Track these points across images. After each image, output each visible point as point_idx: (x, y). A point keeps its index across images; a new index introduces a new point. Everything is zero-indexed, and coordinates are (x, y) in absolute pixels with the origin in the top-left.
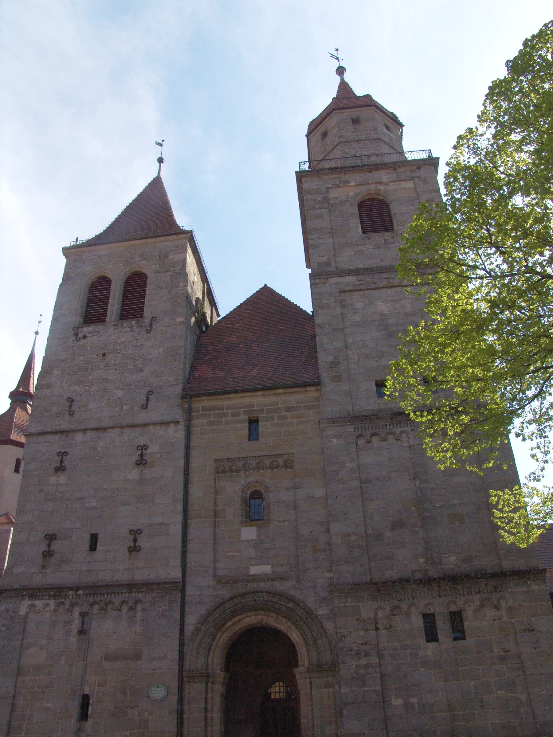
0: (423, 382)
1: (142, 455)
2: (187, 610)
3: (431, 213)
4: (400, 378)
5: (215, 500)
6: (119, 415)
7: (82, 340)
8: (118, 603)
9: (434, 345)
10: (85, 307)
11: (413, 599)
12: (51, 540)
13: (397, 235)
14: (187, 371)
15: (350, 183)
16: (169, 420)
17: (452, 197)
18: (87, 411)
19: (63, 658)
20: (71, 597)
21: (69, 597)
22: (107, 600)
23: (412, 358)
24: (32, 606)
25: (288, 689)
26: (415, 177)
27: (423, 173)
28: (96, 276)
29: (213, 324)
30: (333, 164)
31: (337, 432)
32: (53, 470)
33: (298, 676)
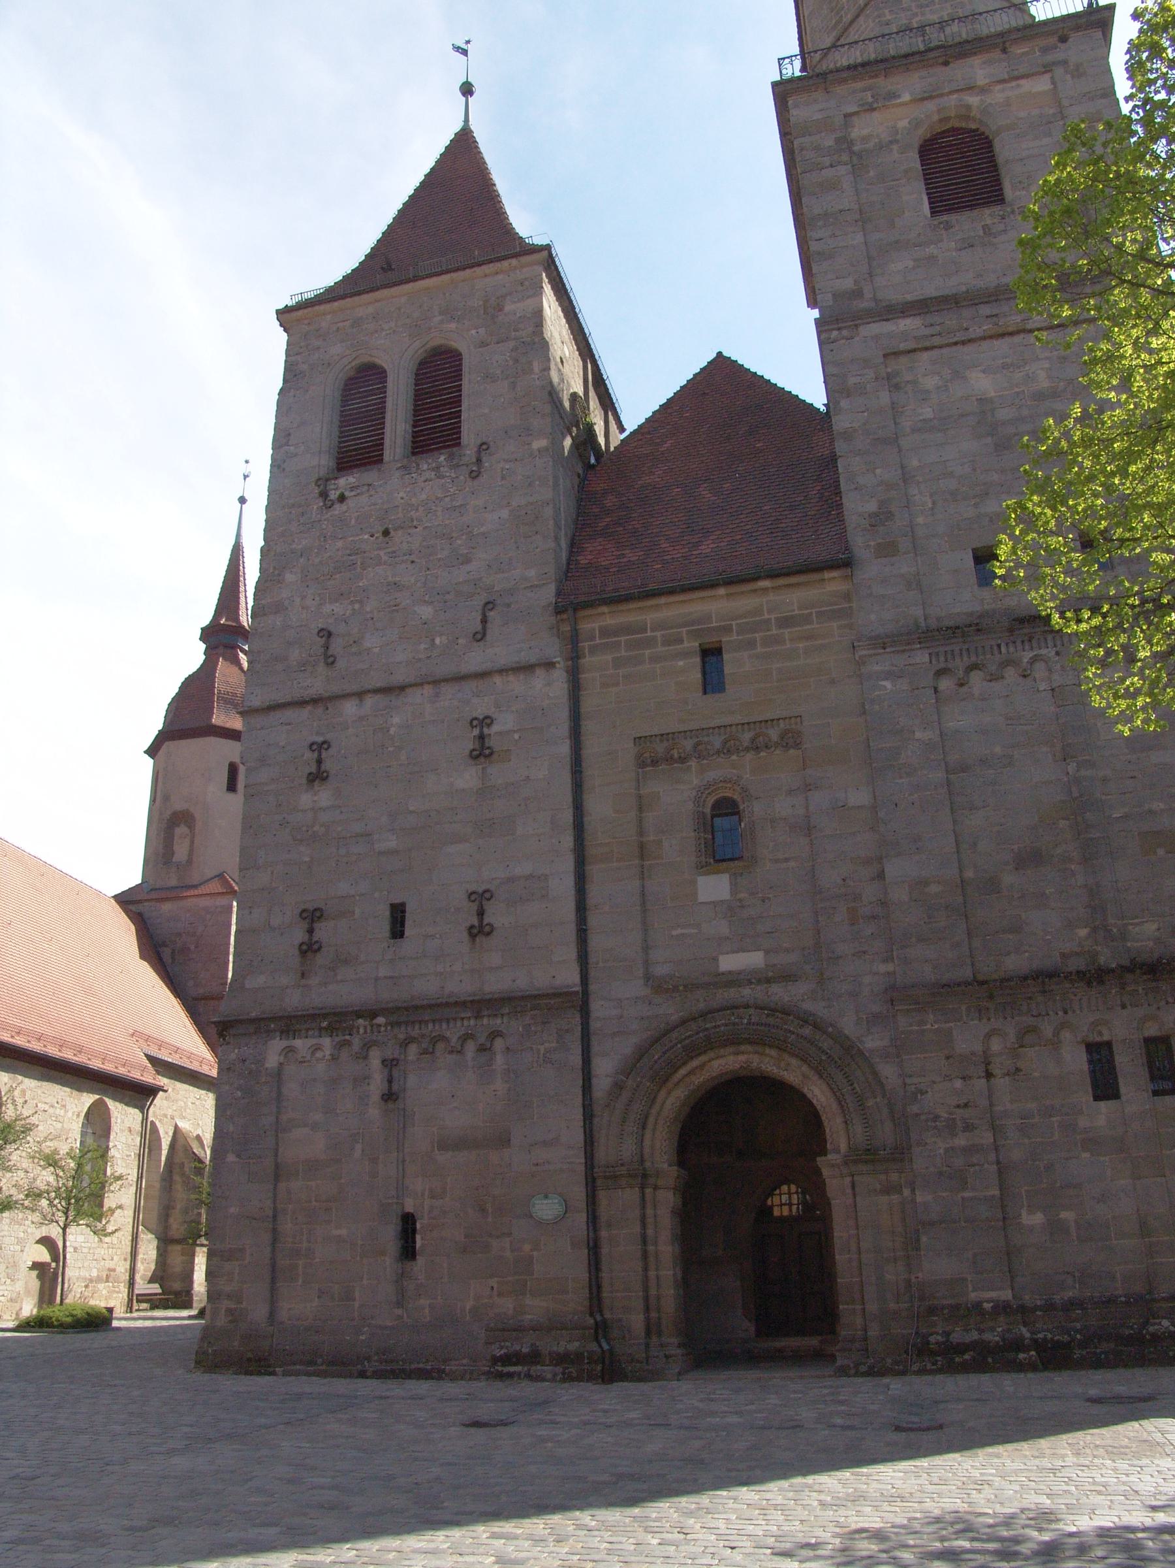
0: (1078, 543)
1: (482, 737)
2: (595, 1048)
3: (1094, 145)
4: (1029, 538)
5: (640, 821)
6: (429, 657)
7: (337, 506)
8: (454, 1040)
9: (1103, 459)
10: (338, 433)
11: (1066, 1012)
12: (313, 921)
13: (1013, 212)
14: (564, 556)
15: (899, 96)
16: (533, 660)
17: (1147, 101)
18: (360, 653)
19: (359, 1147)
20: (362, 1031)
21: (358, 1032)
22: (434, 1034)
23: (1054, 491)
24: (290, 1050)
25: (808, 1197)
26: (1054, 64)
27: (1076, 50)
28: (353, 364)
29: (612, 449)
30: (858, 53)
31: (892, 665)
32: (304, 781)
33: (826, 1172)
